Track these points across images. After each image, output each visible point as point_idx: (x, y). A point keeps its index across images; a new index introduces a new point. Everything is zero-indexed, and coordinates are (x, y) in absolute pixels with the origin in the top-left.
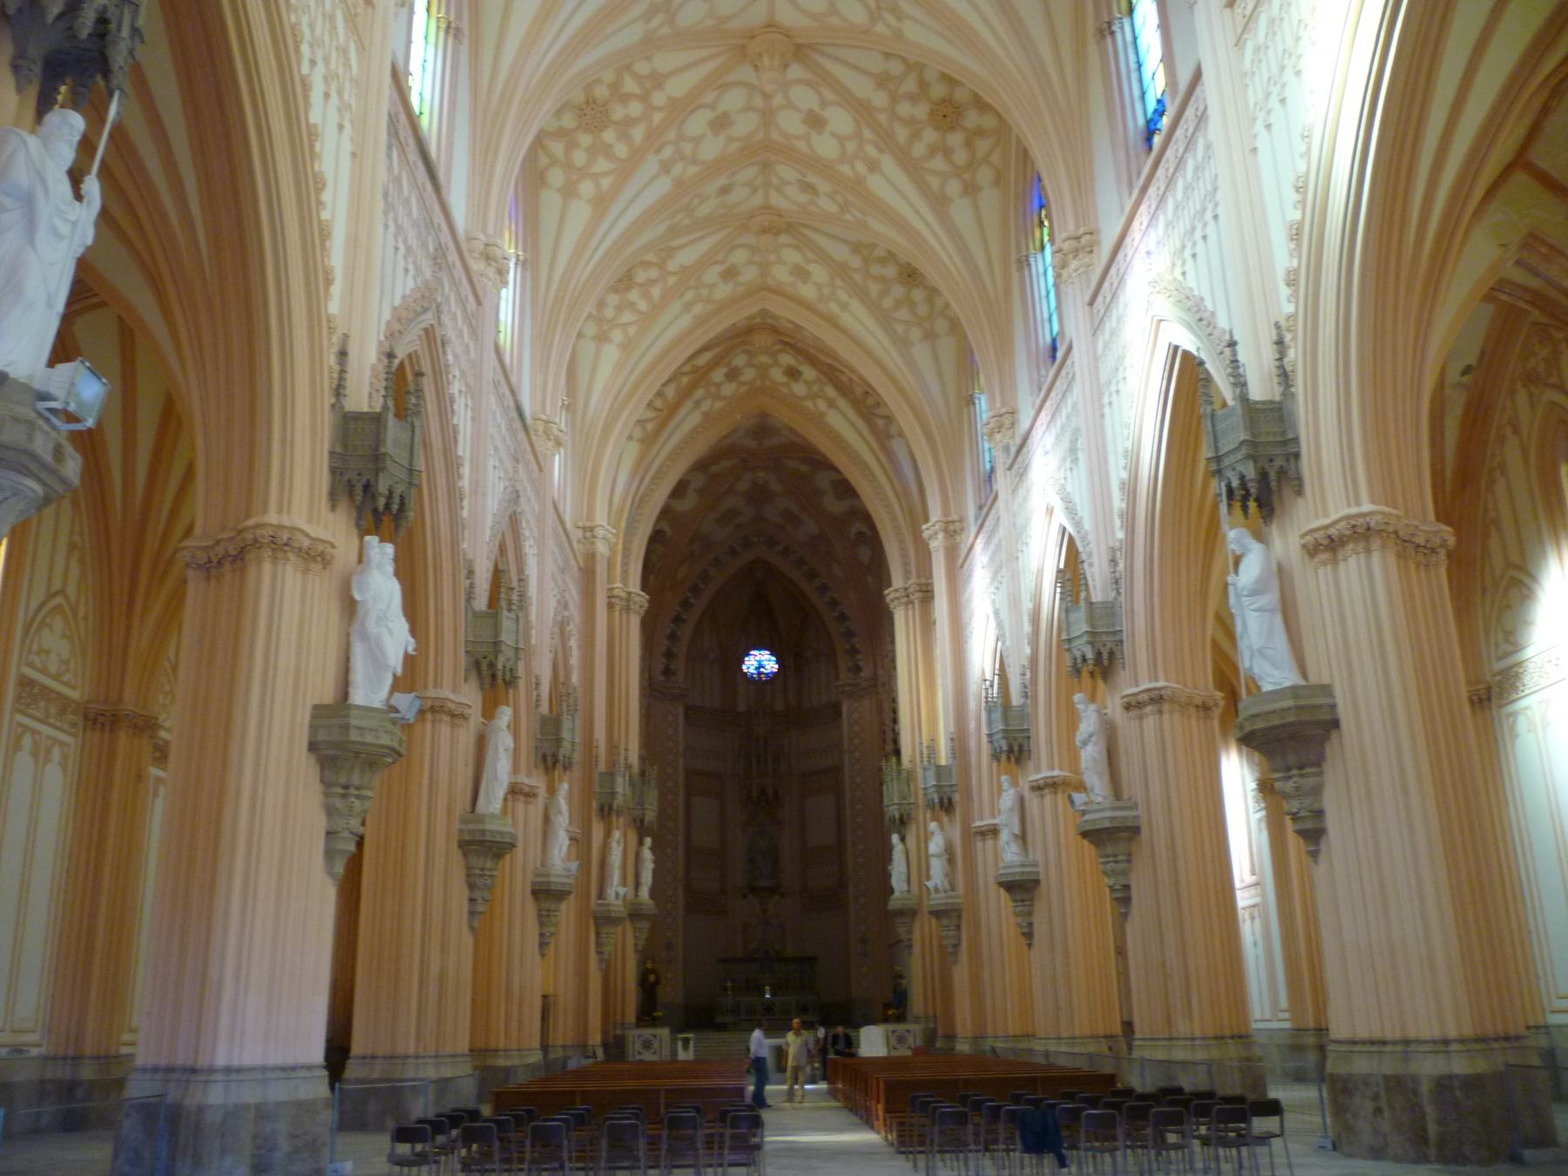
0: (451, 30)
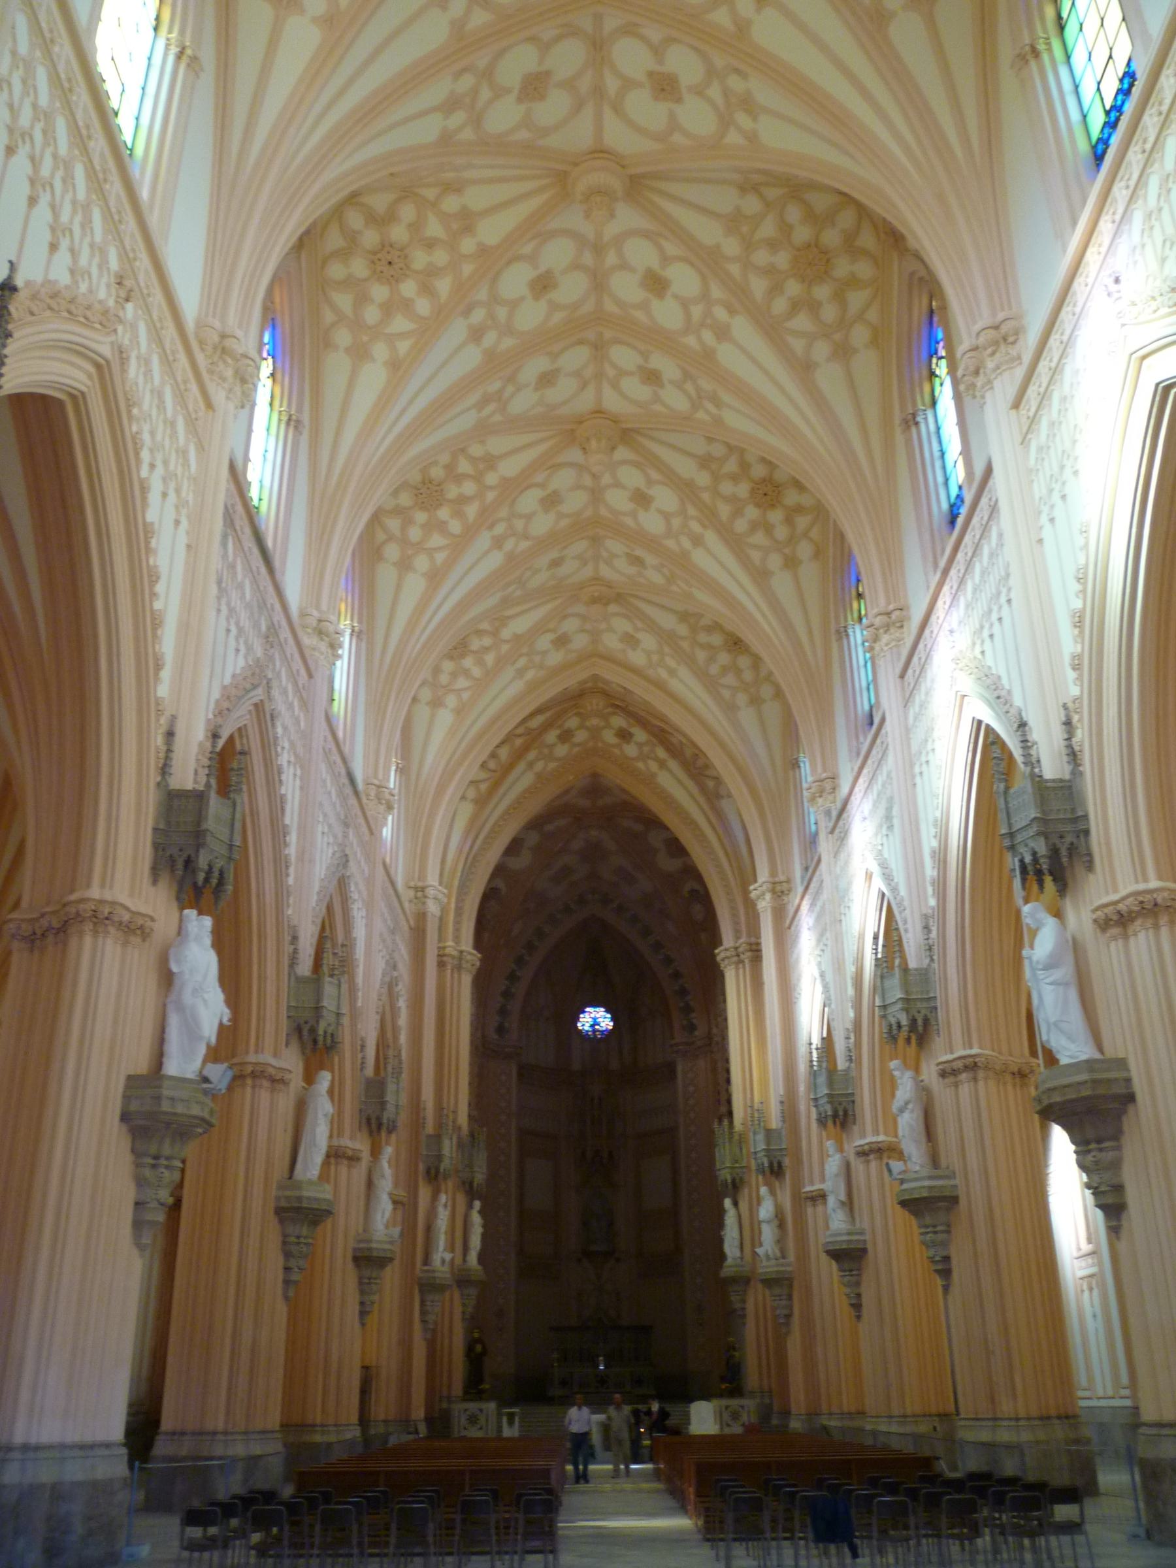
0: (292, 423)
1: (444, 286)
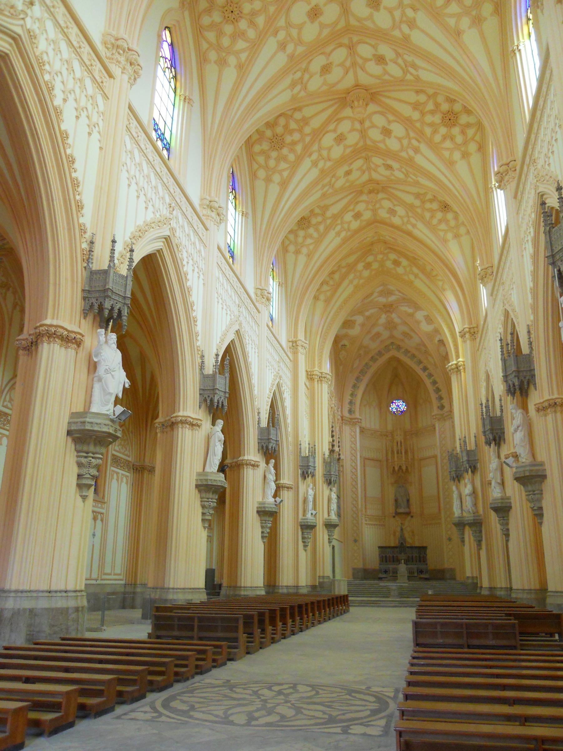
1: (260, 20)
